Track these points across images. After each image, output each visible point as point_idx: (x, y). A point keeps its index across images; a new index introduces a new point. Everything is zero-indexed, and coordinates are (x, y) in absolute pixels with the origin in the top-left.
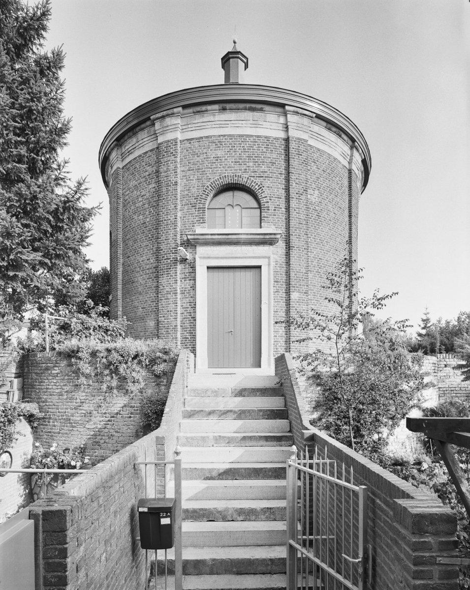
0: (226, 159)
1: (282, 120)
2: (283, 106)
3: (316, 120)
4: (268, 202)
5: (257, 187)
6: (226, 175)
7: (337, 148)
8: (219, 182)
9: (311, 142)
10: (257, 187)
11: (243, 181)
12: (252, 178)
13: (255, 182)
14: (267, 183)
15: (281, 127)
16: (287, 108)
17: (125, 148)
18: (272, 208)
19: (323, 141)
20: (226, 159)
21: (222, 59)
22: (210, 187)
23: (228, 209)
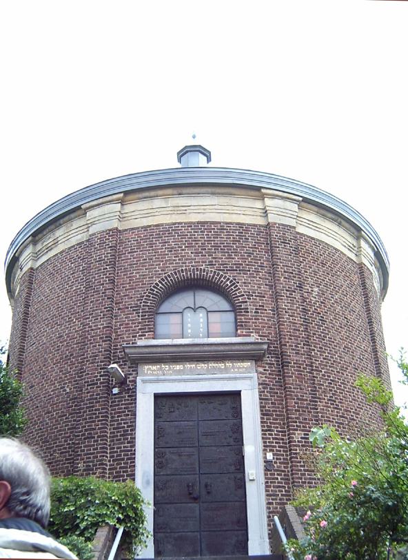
0: (183, 250)
1: (259, 204)
2: (258, 189)
3: (303, 204)
4: (246, 302)
5: (228, 283)
6: (184, 268)
7: (337, 238)
8: (231, 286)
9: (301, 229)
10: (228, 283)
11: (209, 272)
12: (221, 273)
13: (226, 277)
14: (242, 278)
15: (259, 212)
16: (263, 191)
17: (42, 244)
18: (251, 308)
19: (317, 229)
20: (183, 250)
21: (178, 153)
22: (160, 285)
23: (189, 315)
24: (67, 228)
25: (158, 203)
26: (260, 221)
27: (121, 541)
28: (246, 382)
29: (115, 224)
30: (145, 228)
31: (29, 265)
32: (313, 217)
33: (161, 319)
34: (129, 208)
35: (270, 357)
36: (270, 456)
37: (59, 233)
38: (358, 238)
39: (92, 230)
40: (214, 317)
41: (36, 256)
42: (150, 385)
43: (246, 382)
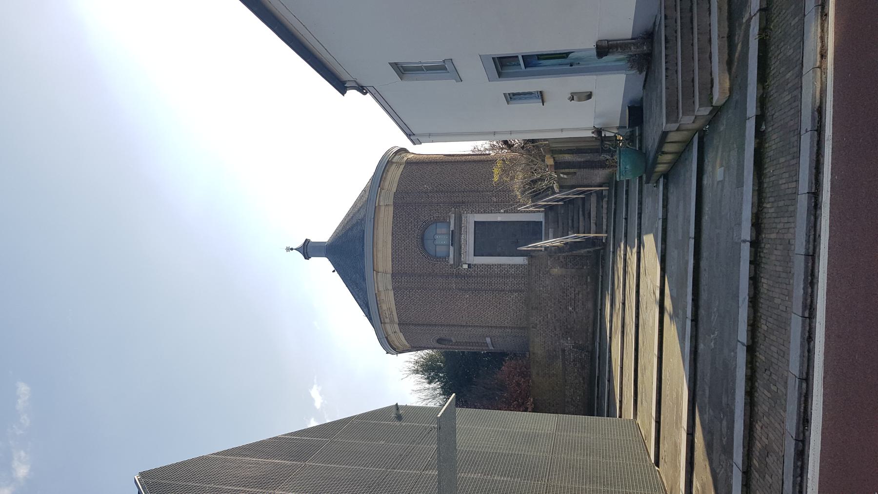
1: (383, 208)
23: (437, 242)
24: (740, 25)
25: (380, 255)
26: (391, 209)
27: (528, 223)
28: (471, 219)
29: (389, 276)
30: (392, 261)
31: (396, 326)
32: (387, 183)
33: (438, 255)
34: (381, 269)
35: (461, 205)
36: (502, 211)
37: (384, 307)
38: (393, 163)
39: (390, 287)
40: (439, 231)
41: (392, 322)
42: (470, 258)
43: (471, 219)
